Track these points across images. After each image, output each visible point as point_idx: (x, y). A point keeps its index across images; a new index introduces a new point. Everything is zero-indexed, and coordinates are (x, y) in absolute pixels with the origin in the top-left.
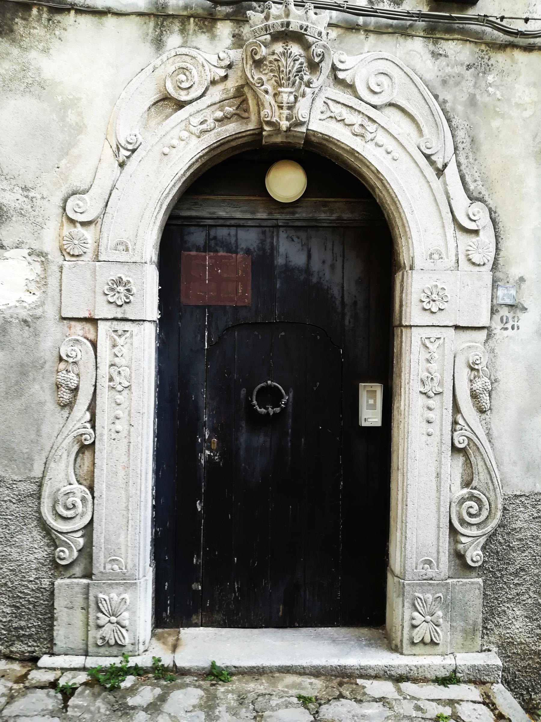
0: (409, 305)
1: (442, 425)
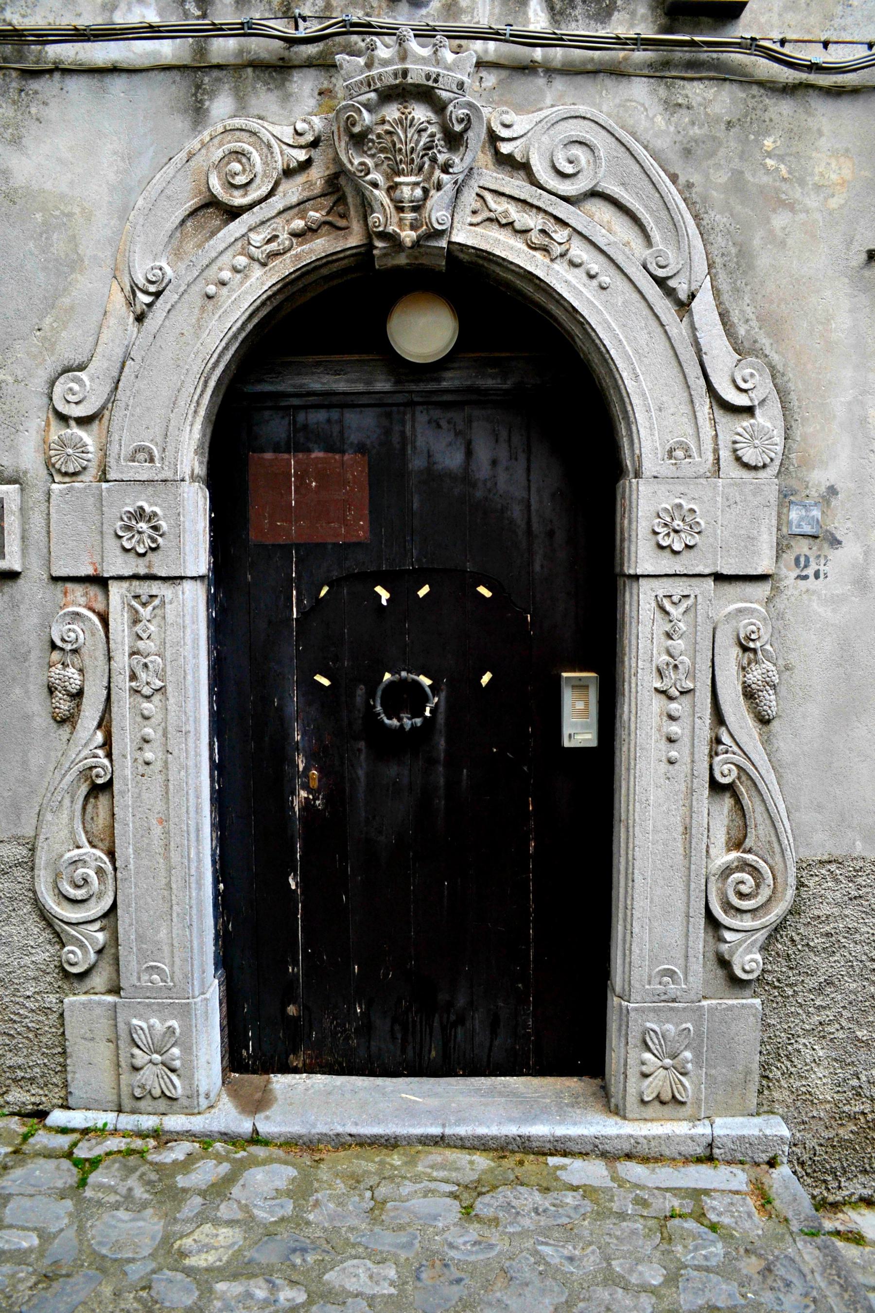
0: (634, 539)
1: (693, 745)
